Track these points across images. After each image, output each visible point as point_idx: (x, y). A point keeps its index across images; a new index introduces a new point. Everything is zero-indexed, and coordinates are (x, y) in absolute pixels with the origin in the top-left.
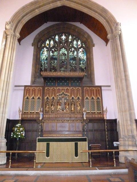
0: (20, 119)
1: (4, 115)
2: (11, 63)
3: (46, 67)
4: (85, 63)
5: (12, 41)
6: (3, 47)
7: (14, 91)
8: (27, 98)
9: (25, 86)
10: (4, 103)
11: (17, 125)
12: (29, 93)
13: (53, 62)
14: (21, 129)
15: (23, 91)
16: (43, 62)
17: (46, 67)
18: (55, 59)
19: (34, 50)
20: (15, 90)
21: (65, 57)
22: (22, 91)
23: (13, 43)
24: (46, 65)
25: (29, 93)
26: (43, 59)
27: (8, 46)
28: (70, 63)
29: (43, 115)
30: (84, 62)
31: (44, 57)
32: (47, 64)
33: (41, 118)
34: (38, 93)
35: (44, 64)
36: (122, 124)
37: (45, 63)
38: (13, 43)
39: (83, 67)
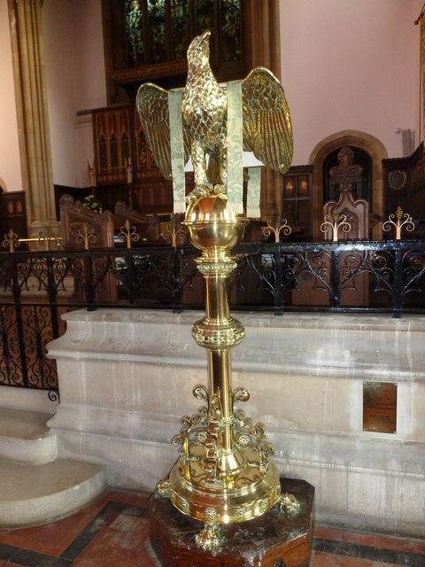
0: (93, 183)
1: (46, 179)
2: (38, 69)
3: (141, 49)
4: (238, 16)
5: (28, 10)
6: (14, 31)
7: (78, 126)
8: (102, 138)
9: (94, 112)
10: (42, 158)
11: (87, 198)
12: (104, 128)
13: (155, 32)
14: (95, 204)
15: (91, 124)
16: (133, 37)
17: (141, 49)
18: (158, 21)
19: (102, 8)
20: (79, 123)
21: (184, 10)
22: (87, 124)
23: (31, 14)
24: (140, 43)
25: (104, 128)
26: (133, 27)
27: (23, 28)
28: (198, 23)
29: (134, 174)
30: (236, 13)
31: (134, 19)
32: (142, 40)
33: (130, 180)
34: (121, 124)
35: (136, 41)
36: (41, 212)
37: (137, 37)
38: (31, 14)
39: (232, 30)
